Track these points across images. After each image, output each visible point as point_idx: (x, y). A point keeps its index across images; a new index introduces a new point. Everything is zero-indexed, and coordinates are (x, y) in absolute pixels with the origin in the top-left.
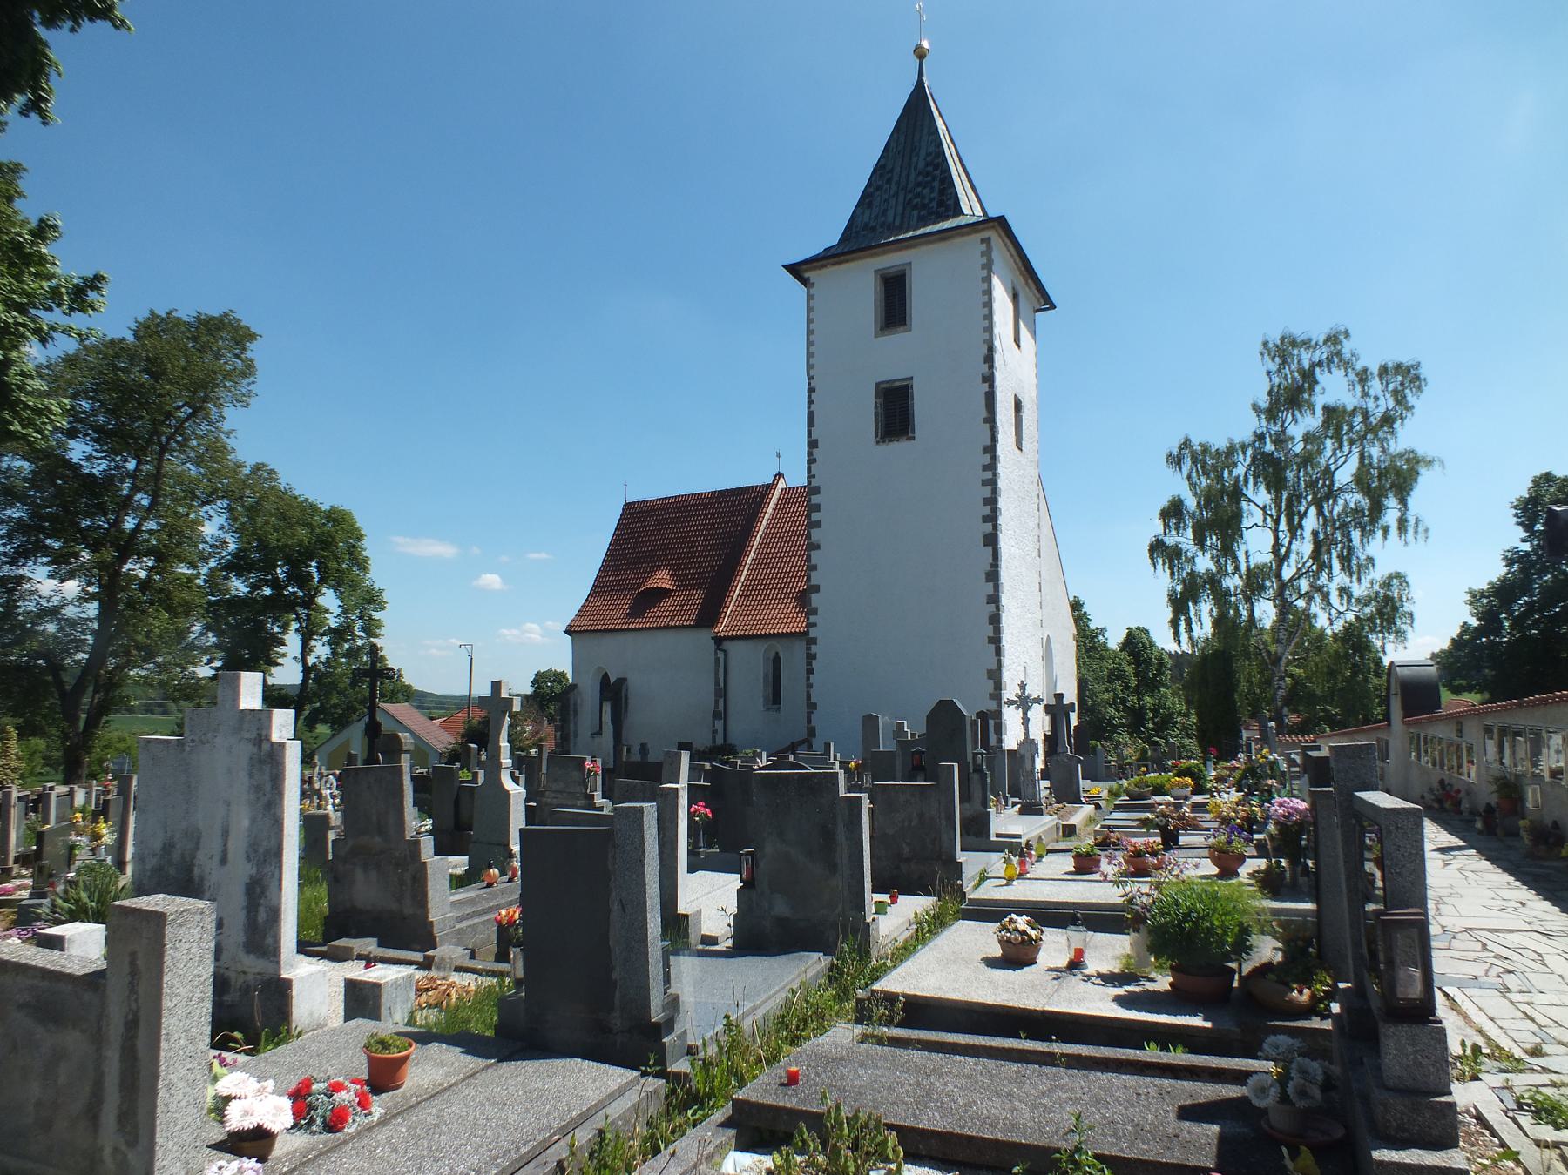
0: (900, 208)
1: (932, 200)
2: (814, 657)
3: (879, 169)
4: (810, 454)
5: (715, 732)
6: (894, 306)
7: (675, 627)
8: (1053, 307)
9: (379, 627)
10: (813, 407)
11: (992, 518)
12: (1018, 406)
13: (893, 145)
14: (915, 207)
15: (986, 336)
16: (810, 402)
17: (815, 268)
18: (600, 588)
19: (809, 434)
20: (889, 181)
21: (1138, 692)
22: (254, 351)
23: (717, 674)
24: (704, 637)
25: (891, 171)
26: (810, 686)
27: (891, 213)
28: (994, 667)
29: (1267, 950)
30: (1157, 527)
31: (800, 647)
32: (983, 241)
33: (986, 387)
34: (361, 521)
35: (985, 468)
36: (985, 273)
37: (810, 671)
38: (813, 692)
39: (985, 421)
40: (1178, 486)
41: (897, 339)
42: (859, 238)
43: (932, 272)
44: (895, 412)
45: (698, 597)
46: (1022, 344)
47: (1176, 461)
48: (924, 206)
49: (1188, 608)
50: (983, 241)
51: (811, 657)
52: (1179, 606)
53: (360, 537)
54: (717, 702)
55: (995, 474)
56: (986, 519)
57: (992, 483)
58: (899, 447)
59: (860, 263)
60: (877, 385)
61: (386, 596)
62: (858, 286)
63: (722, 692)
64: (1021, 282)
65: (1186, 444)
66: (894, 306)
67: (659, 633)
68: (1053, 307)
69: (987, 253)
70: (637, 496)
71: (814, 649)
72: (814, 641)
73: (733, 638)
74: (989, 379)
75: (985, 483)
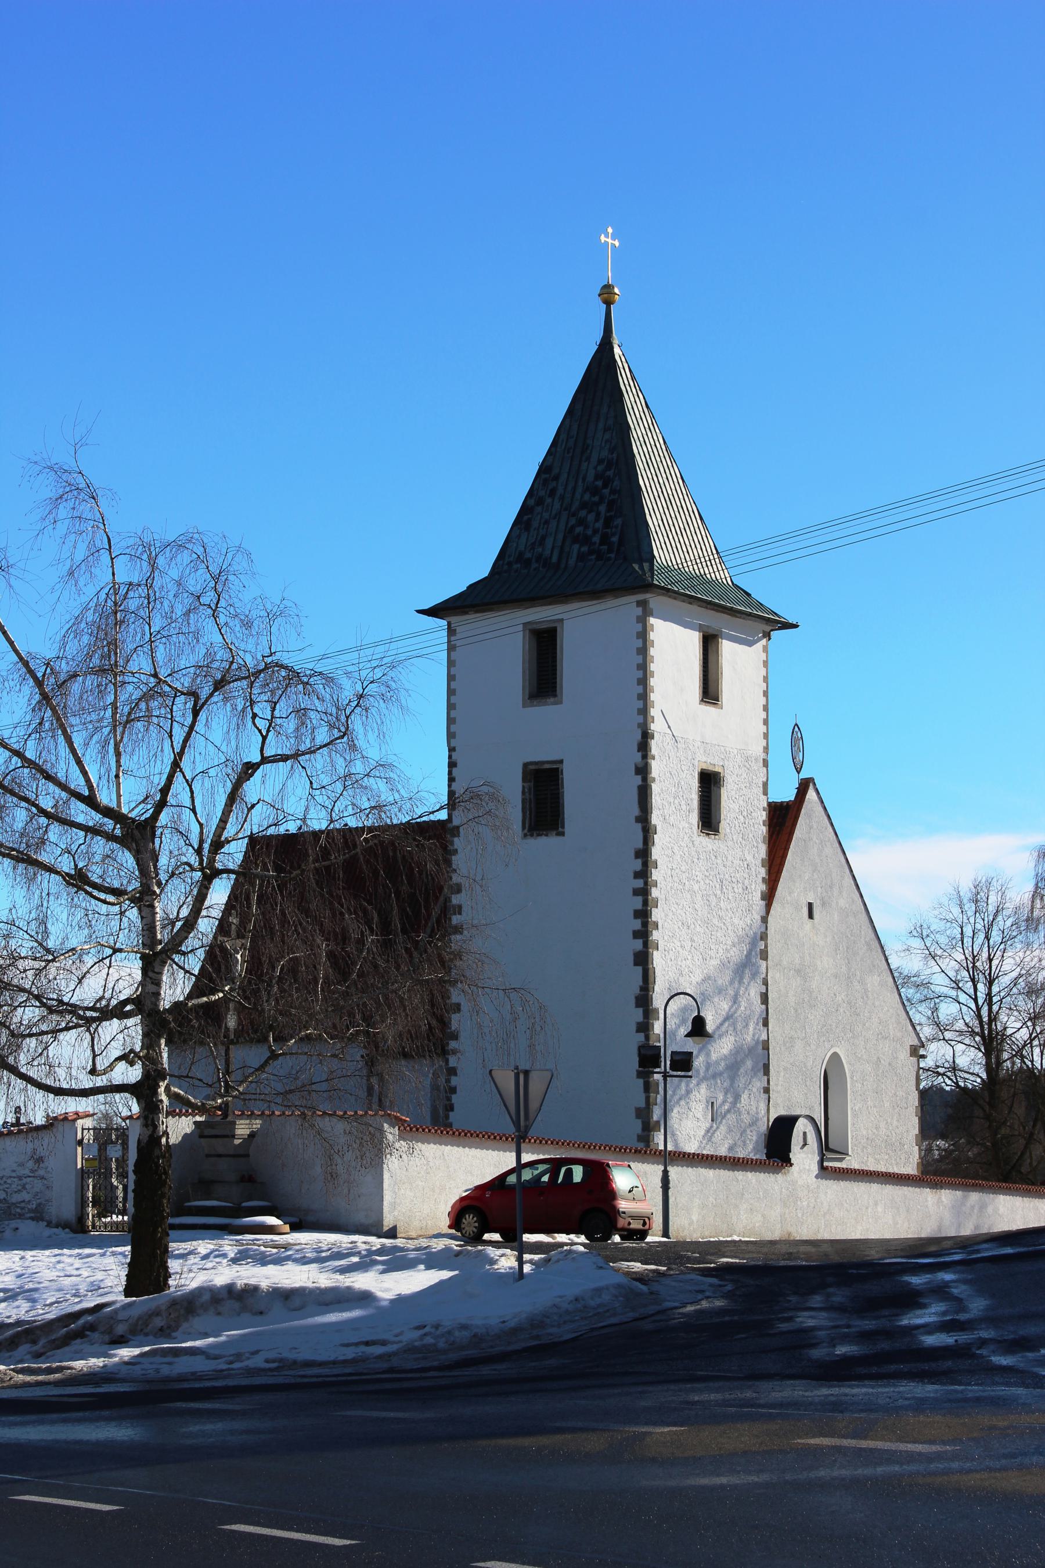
0: (560, 536)
1: (595, 531)
2: (453, 1090)
3: (544, 469)
4: (450, 773)
6: (544, 680)
11: (644, 932)
13: (563, 436)
14: (576, 540)
15: (640, 719)
25: (556, 478)
27: (549, 542)
29: (545, 1178)
33: (638, 780)
39: (638, 820)
41: (545, 712)
43: (585, 627)
44: (544, 798)
48: (586, 540)
50: (639, 603)
55: (646, 883)
60: (526, 765)
62: (506, 634)
66: (544, 680)
74: (643, 771)
75: (636, 892)
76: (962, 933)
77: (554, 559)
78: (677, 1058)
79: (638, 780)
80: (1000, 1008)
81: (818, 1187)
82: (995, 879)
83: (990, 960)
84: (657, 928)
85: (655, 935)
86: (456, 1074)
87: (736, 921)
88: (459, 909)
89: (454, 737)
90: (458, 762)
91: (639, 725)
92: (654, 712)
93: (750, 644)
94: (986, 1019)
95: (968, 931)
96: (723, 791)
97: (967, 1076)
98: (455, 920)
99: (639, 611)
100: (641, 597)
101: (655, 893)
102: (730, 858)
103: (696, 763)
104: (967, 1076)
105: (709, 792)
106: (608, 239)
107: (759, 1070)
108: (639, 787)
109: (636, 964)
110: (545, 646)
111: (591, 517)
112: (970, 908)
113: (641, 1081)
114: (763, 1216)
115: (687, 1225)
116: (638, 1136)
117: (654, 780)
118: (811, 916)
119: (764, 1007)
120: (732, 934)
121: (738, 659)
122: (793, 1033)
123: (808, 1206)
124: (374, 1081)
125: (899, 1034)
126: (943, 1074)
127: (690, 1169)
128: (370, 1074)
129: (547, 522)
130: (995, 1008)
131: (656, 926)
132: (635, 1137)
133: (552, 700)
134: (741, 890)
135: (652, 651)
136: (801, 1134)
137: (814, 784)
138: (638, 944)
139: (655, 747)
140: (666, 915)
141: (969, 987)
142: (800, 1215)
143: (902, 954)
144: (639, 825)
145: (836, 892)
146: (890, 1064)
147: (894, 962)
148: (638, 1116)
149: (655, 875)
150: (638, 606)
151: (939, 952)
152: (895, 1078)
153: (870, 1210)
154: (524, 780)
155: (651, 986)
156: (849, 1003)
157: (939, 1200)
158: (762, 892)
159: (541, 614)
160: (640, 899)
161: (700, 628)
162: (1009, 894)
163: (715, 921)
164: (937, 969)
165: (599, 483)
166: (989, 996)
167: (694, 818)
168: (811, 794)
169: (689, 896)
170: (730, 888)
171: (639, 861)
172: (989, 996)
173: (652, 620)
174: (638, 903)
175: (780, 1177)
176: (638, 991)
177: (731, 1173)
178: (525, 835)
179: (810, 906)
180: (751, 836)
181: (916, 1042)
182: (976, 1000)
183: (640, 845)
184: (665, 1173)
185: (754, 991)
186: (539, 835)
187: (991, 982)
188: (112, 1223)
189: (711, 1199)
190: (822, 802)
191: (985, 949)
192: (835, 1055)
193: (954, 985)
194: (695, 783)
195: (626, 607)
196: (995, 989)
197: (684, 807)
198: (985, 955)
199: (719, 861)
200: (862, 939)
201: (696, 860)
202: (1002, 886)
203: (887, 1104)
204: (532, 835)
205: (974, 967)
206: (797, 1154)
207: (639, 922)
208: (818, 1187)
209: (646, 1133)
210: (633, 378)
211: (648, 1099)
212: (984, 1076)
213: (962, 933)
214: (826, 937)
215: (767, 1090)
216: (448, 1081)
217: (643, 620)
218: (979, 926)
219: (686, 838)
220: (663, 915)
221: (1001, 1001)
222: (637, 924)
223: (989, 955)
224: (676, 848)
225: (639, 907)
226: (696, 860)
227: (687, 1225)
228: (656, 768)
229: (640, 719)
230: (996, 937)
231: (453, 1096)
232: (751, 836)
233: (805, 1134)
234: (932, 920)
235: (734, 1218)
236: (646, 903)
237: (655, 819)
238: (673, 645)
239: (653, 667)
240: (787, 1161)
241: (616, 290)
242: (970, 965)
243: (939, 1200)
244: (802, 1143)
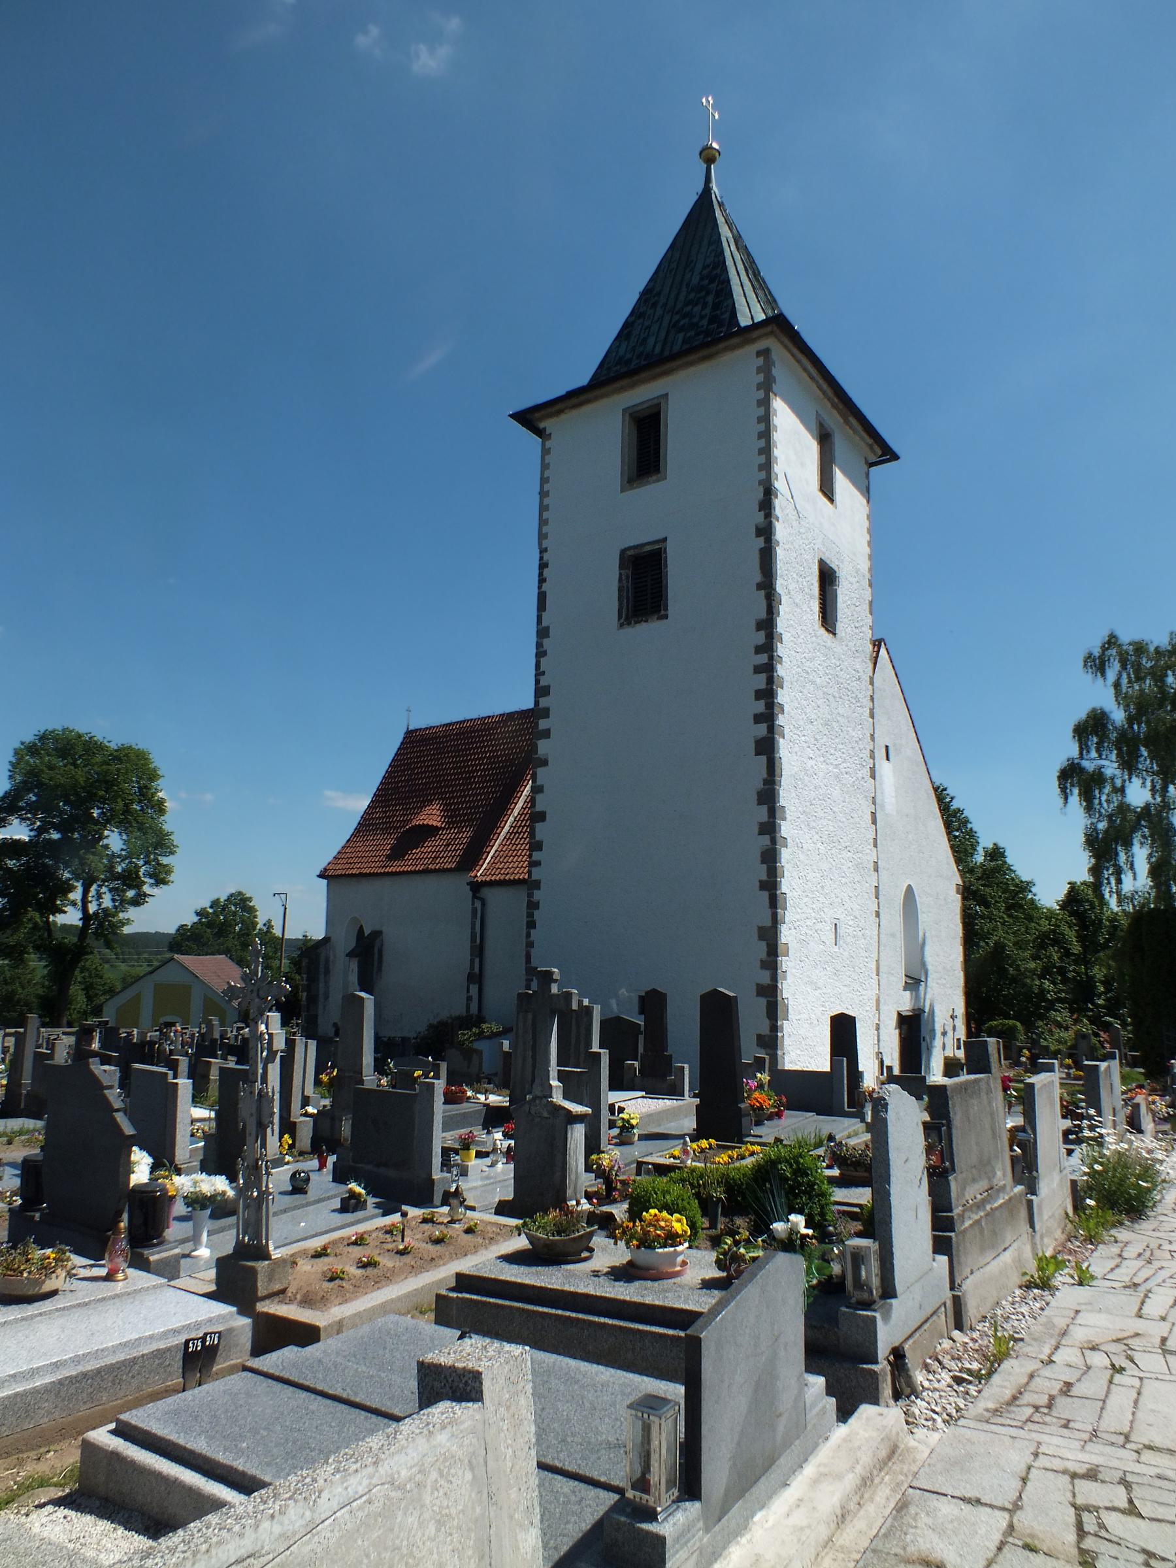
1: (702, 317)
4: (539, 645)
5: (469, 999)
6: (646, 453)
7: (435, 871)
8: (895, 457)
9: (169, 872)
10: (545, 587)
11: (768, 716)
12: (827, 578)
16: (542, 580)
17: (551, 416)
18: (367, 825)
19: (539, 620)
20: (654, 305)
21: (1082, 960)
22: (966, 813)
23: (473, 928)
24: (457, 886)
25: (659, 294)
26: (530, 945)
28: (769, 923)
30: (1072, 749)
31: (519, 897)
32: (759, 354)
34: (158, 760)
35: (759, 650)
36: (761, 394)
37: (531, 925)
38: (533, 952)
39: (760, 587)
40: (1101, 695)
41: (639, 536)
42: (614, 372)
43: (693, 399)
44: (644, 584)
45: (467, 834)
46: (838, 497)
47: (1097, 664)
49: (1117, 854)
50: (759, 354)
51: (533, 906)
52: (1104, 848)
53: (153, 776)
54: (472, 962)
55: (771, 658)
56: (758, 718)
57: (768, 669)
59: (604, 402)
60: (623, 552)
61: (176, 839)
63: (478, 950)
64: (834, 420)
65: (1112, 641)
66: (646, 453)
67: (417, 879)
68: (895, 457)
69: (766, 370)
70: (420, 721)
71: (537, 895)
72: (537, 885)
73: (491, 884)
74: (766, 532)
75: (758, 670)
84: (783, 712)
85: (781, 720)
86: (539, 888)
91: (760, 483)
108: (761, 550)
109: (758, 753)
113: (766, 894)
124: (478, 904)
128: (474, 897)
129: (649, 327)
133: (654, 478)
149: (781, 650)
154: (621, 567)
155: (777, 778)
159: (641, 394)
160: (763, 676)
165: (706, 282)
171: (762, 634)
174: (760, 681)
176: (761, 786)
178: (622, 625)
183: (763, 615)
188: (1146, 1182)
204: (629, 624)
207: (762, 703)
209: (772, 958)
225: (763, 686)
228: (781, 531)
231: (536, 912)
237: (780, 586)
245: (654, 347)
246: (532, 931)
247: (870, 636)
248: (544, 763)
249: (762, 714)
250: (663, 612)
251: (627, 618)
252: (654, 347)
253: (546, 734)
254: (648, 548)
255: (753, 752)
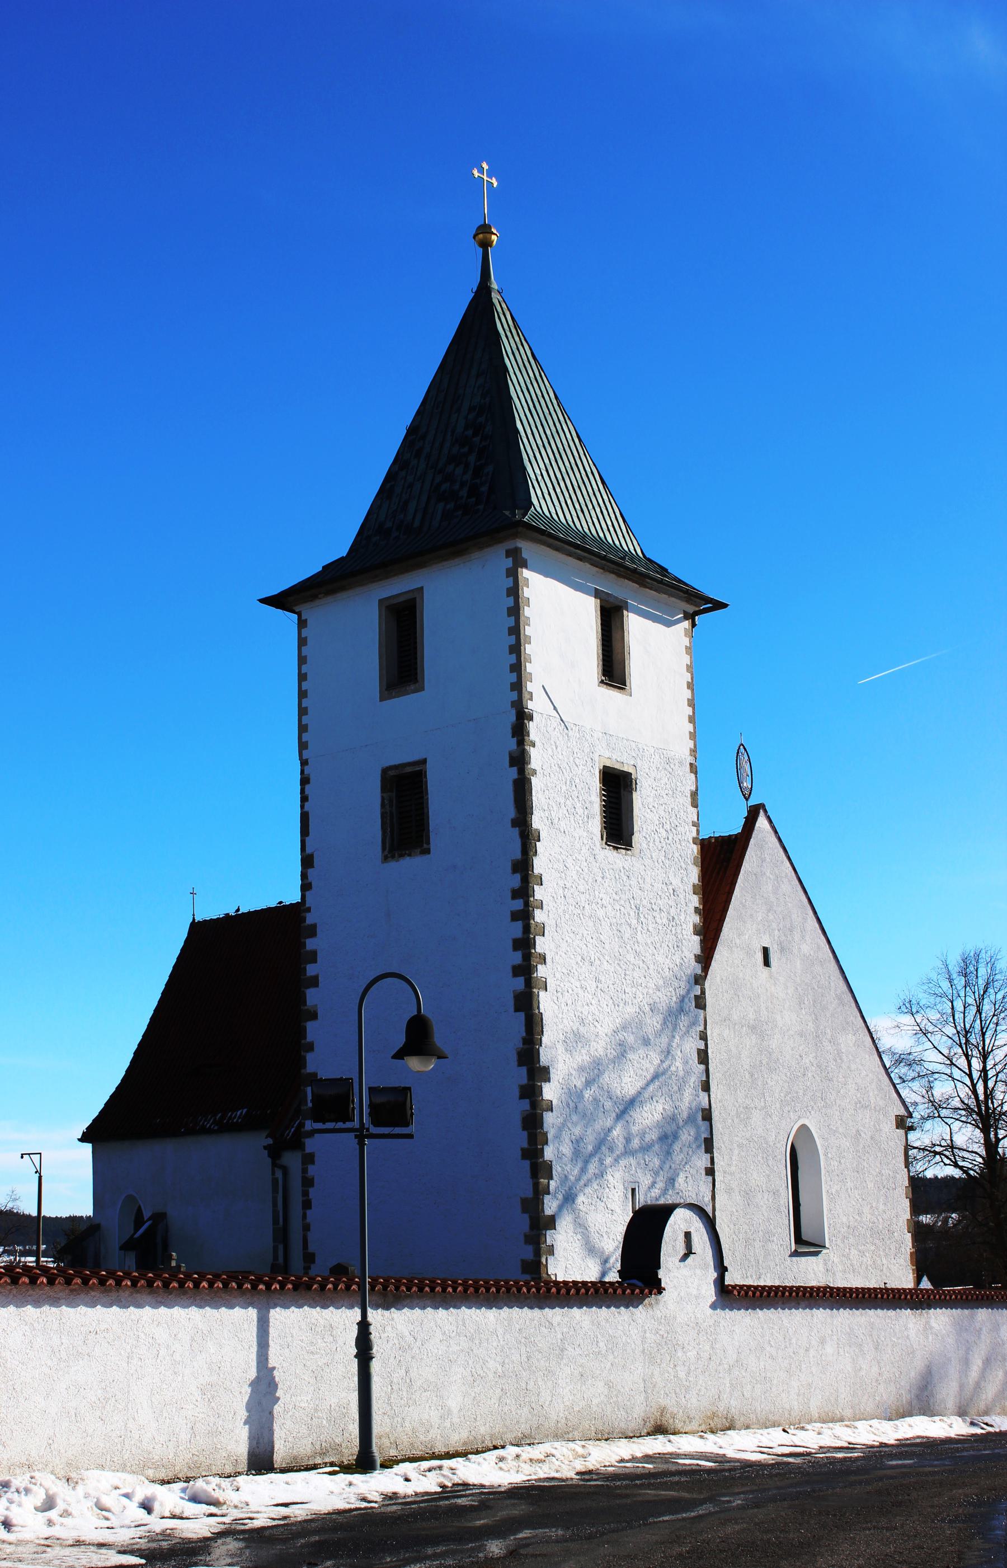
3: (412, 431)
6: (402, 665)
15: (514, 696)
16: (304, 799)
33: (513, 773)
38: (311, 1236)
41: (406, 703)
43: (447, 593)
44: (405, 809)
50: (509, 553)
54: (275, 1249)
55: (527, 904)
58: (410, 865)
60: (385, 771)
62: (357, 620)
66: (402, 665)
70: (211, 910)
74: (519, 760)
75: (515, 916)
76: (953, 1008)
77: (417, 524)
78: (380, 1099)
79: (513, 773)
80: (996, 1082)
81: (717, 1323)
82: (983, 951)
83: (983, 1034)
86: (313, 1162)
87: (660, 959)
88: (313, 957)
89: (306, 748)
90: (312, 777)
92: (530, 687)
93: (669, 624)
94: (982, 1097)
95: (959, 1005)
96: (636, 796)
97: (966, 1155)
98: (311, 970)
99: (509, 562)
100: (510, 545)
101: (539, 916)
102: (648, 880)
103: (597, 758)
104: (966, 1155)
105: (619, 798)
106: (482, 173)
107: (699, 1147)
110: (403, 624)
111: (459, 470)
112: (960, 982)
113: (527, 1164)
114: (609, 1385)
115: (435, 1420)
116: (526, 1236)
117: (534, 772)
118: (767, 963)
119: (702, 1067)
120: (654, 974)
121: (656, 643)
122: (748, 1102)
123: (699, 1357)
124: (279, 1174)
125: (881, 1103)
126: (940, 1153)
127: (441, 1312)
128: (274, 1165)
130: (991, 1084)
131: (543, 959)
132: (522, 1238)
133: (412, 687)
134: (665, 921)
135: (527, 612)
136: (681, 1238)
137: (766, 811)
138: (519, 983)
139: (534, 729)
140: (558, 946)
141: (962, 1062)
142: (682, 1375)
143: (892, 1031)
144: (516, 831)
145: (797, 936)
146: (872, 1138)
147: (884, 1044)
148: (524, 1210)
149: (539, 893)
150: (507, 556)
151: (931, 1028)
152: (879, 1155)
153: (812, 1352)
154: (384, 788)
156: (819, 1066)
157: (927, 1327)
158: (695, 926)
159: (397, 587)
160: (519, 924)
161: (597, 594)
162: (1000, 965)
163: (630, 957)
164: (929, 1045)
166: (984, 1071)
167: (596, 825)
168: (762, 822)
169: (591, 924)
170: (650, 918)
171: (518, 877)
172: (984, 1071)
173: (525, 573)
175: (640, 1313)
177: (536, 1312)
179: (766, 951)
180: (677, 855)
181: (902, 1112)
182: (970, 1076)
184: (364, 1326)
185: (692, 1045)
186: (401, 856)
187: (985, 1056)
189: (491, 1364)
190: (776, 832)
191: (978, 1021)
192: (804, 1128)
193: (948, 1062)
194: (595, 784)
195: (493, 561)
196: (990, 1063)
197: (580, 811)
198: (977, 1025)
199: (633, 882)
200: (832, 993)
201: (599, 879)
202: (991, 957)
203: (870, 1185)
204: (393, 857)
205: (967, 1041)
206: (671, 1270)
208: (717, 1323)
210: (516, 326)
211: (536, 1185)
212: (983, 1153)
213: (953, 1008)
214: (787, 988)
215: (710, 1172)
216: (305, 1171)
217: (513, 574)
218: (970, 1000)
219: (584, 850)
220: (552, 946)
221: (997, 1075)
222: (517, 958)
223: (982, 1028)
224: (570, 862)
226: (599, 879)
227: (435, 1420)
228: (537, 758)
229: (514, 696)
230: (987, 1008)
231: (311, 1190)
232: (677, 855)
233: (688, 1235)
234: (921, 995)
235: (546, 1397)
236: (527, 929)
237: (537, 821)
238: (558, 614)
239: (528, 631)
240: (655, 1286)
241: (494, 230)
242: (963, 1041)
243: (927, 1327)
244: (682, 1250)
245: (414, 518)
246: (308, 1212)
247: (694, 834)
248: (314, 1016)
249: (519, 966)
250: (425, 846)
251: (390, 851)
252: (414, 518)
253: (314, 982)
254: (409, 769)
255: (512, 1009)
